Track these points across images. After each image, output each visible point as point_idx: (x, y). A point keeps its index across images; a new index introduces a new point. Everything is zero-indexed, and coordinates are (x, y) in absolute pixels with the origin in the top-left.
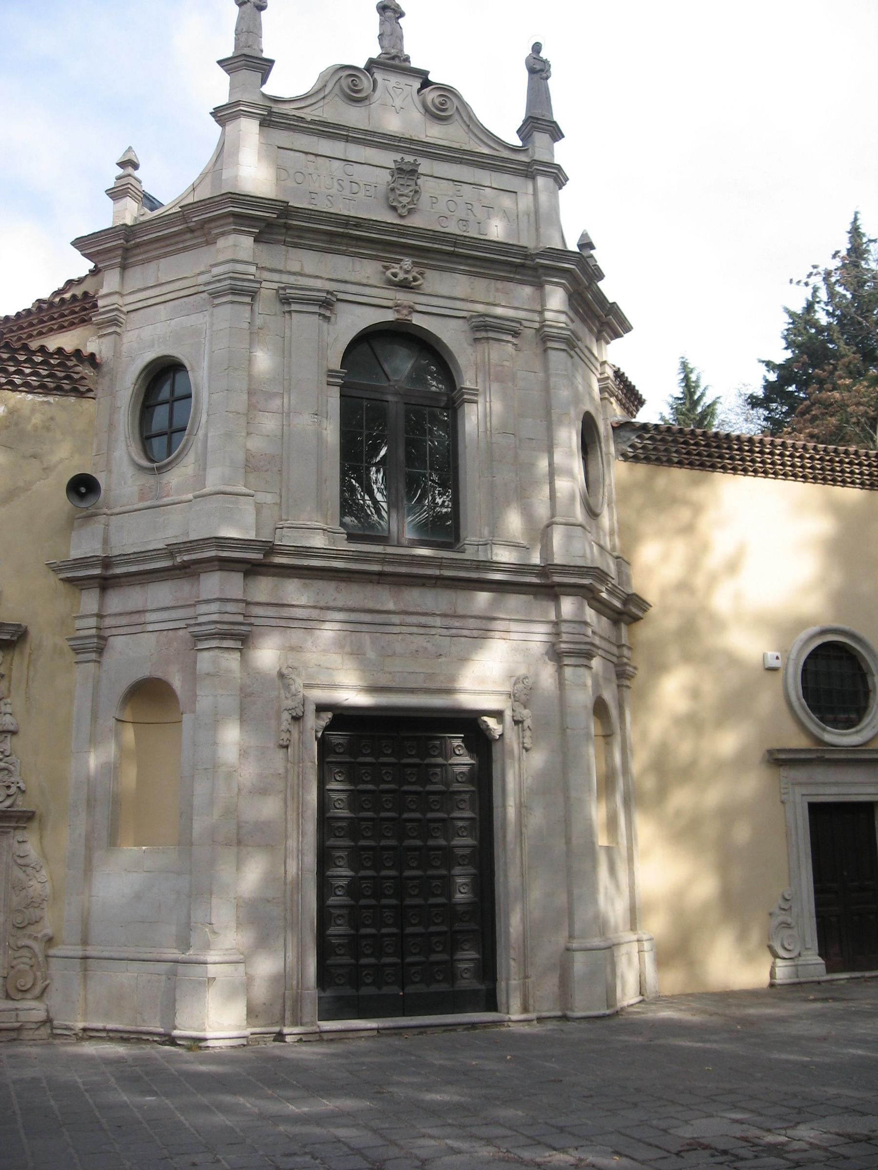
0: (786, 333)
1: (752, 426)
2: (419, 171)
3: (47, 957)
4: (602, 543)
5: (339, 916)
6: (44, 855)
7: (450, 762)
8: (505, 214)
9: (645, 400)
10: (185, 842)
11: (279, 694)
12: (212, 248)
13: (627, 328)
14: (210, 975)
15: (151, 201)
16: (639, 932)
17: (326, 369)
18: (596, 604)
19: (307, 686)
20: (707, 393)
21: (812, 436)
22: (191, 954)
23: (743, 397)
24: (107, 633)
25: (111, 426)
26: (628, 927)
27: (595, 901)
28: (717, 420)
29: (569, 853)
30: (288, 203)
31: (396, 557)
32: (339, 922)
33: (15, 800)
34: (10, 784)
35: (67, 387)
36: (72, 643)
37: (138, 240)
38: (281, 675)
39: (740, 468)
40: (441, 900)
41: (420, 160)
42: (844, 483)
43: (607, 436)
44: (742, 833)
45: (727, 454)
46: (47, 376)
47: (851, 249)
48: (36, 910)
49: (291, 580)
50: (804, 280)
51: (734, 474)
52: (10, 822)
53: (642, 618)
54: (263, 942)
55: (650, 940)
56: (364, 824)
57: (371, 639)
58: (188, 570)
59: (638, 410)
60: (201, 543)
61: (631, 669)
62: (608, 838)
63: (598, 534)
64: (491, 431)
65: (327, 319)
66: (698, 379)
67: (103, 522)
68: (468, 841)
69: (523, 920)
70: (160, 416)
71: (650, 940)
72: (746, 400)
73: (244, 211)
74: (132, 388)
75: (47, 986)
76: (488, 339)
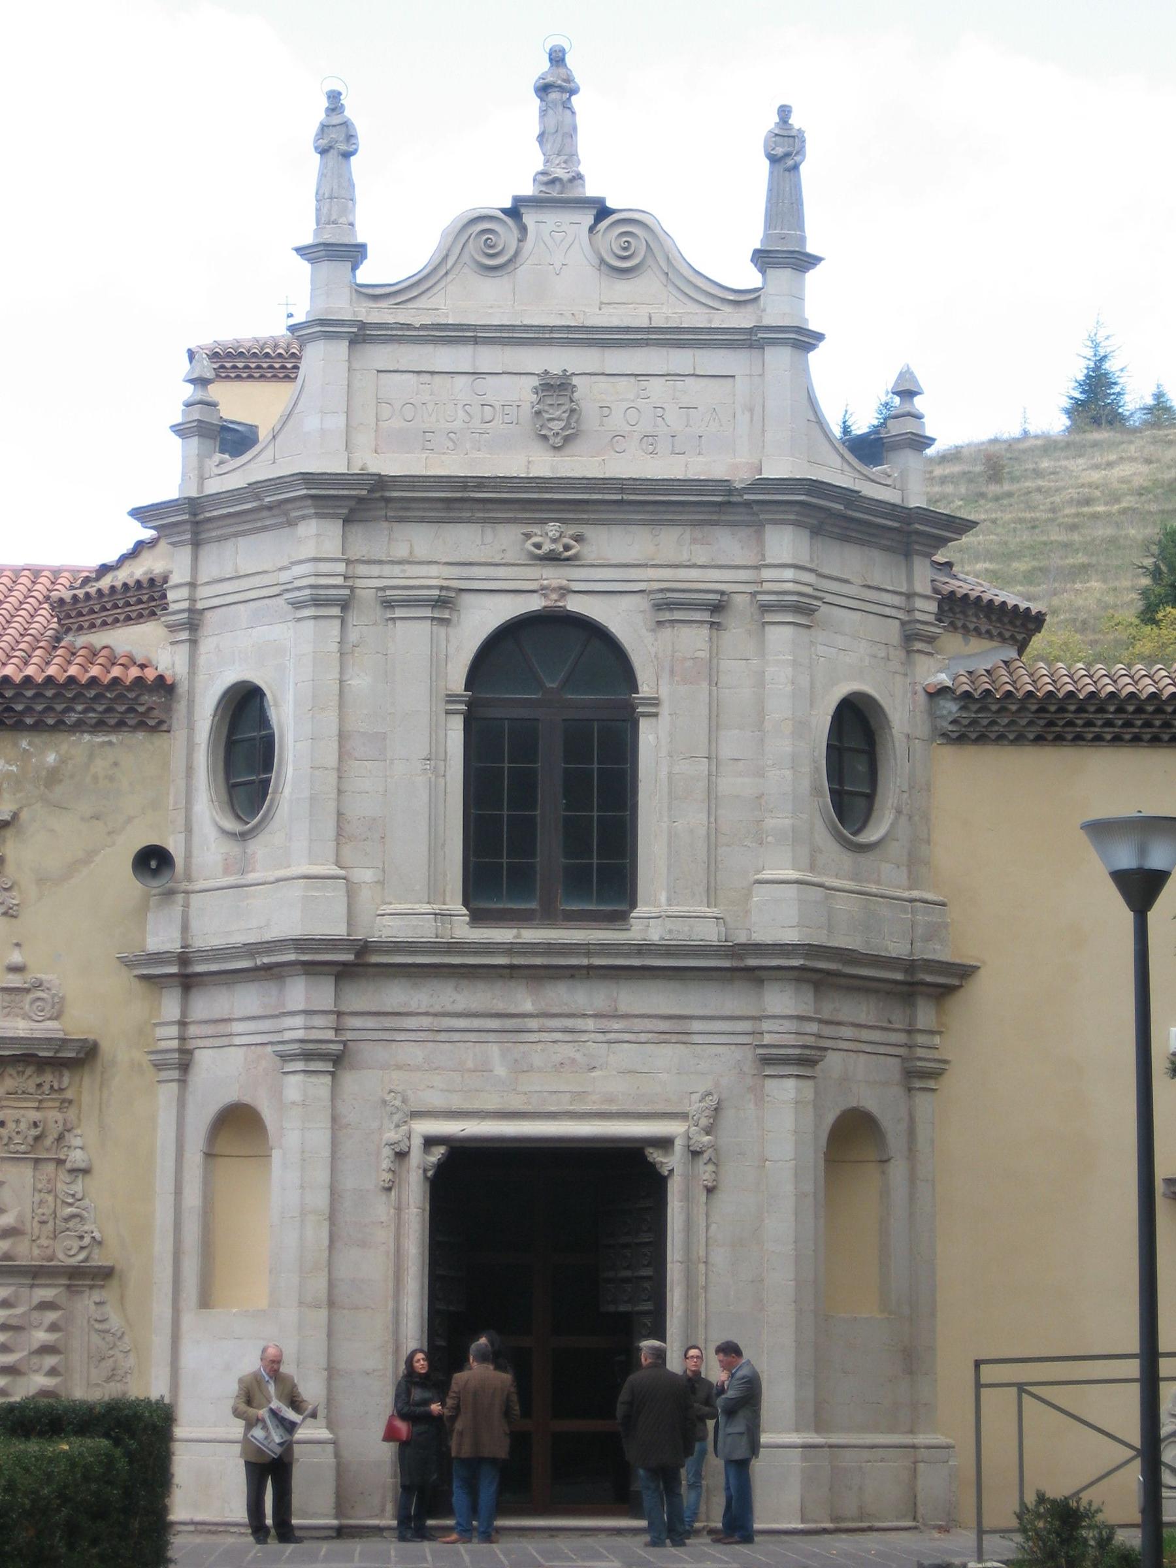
24: (191, 1044)
34: (83, 1234)
36: (153, 1057)
60: (279, 944)
76: (673, 622)
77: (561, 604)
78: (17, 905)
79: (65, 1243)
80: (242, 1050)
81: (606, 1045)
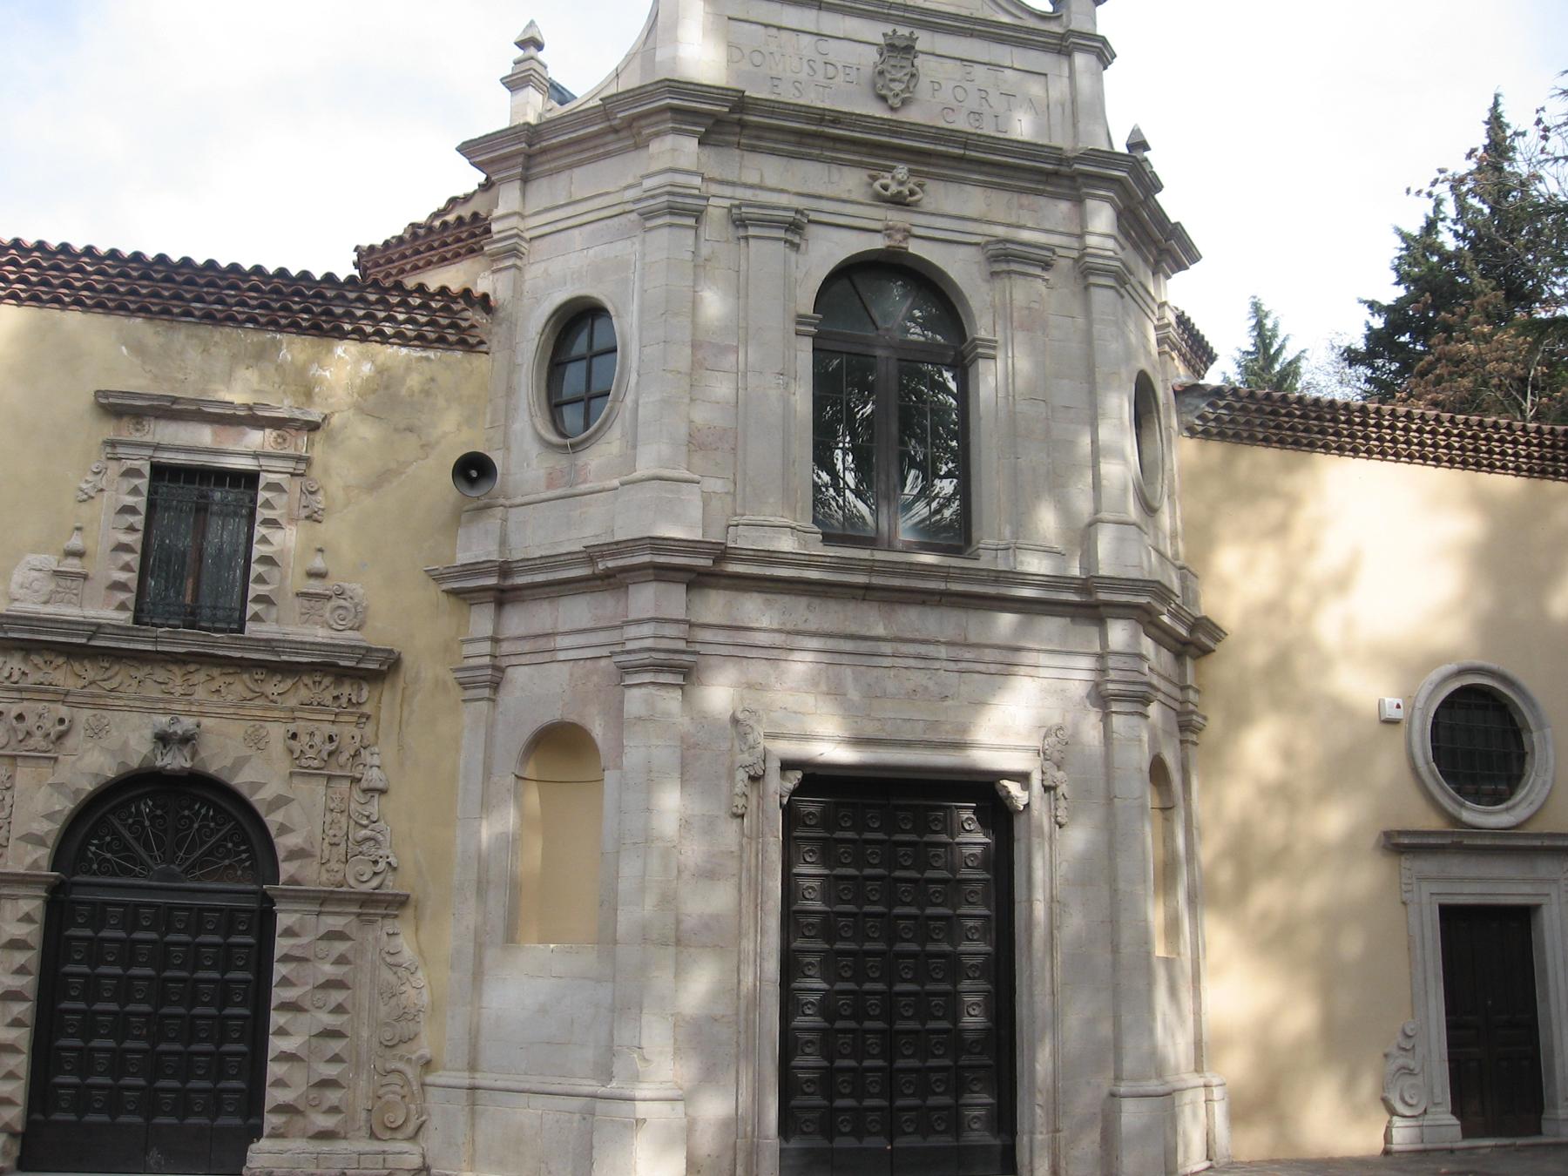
0: (1396, 262)
1: (1348, 390)
2: (917, 48)
3: (423, 1085)
4: (1161, 548)
5: (808, 1042)
6: (421, 953)
7: (957, 840)
8: (1031, 103)
9: (1216, 355)
10: (607, 940)
11: (732, 745)
12: (643, 154)
13: (1194, 256)
14: (640, 1115)
15: (559, 91)
16: (1207, 1074)
17: (793, 315)
18: (1153, 630)
19: (768, 736)
20: (1288, 344)
21: (1435, 404)
22: (613, 1087)
23: (1336, 351)
24: (504, 662)
25: (510, 391)
26: (1192, 1067)
27: (1151, 1031)
28: (1300, 382)
29: (1115, 966)
30: (744, 92)
31: (888, 565)
32: (807, 1050)
33: (384, 880)
34: (377, 858)
35: (432, 336)
37: (544, 144)
38: (735, 721)
39: (1348, 447)
40: (944, 1025)
41: (918, 33)
42: (1492, 468)
43: (1167, 404)
44: (1352, 945)
45: (1330, 427)
46: (427, 324)
47: (1489, 144)
48: (410, 1024)
49: (747, 595)
50: (1427, 189)
51: (1340, 455)
52: (377, 907)
53: (1214, 651)
54: (709, 1075)
55: (1221, 1085)
56: (842, 922)
57: (853, 673)
58: (612, 580)
59: (1207, 368)
60: (631, 544)
61: (1200, 720)
62: (1166, 946)
63: (1156, 536)
64: (1014, 396)
65: (795, 247)
66: (1276, 326)
67: (500, 515)
68: (982, 947)
69: (1054, 1054)
70: (574, 378)
71: (1221, 1085)
72: (1342, 355)
73: (686, 104)
74: (537, 340)
75: (424, 1122)
76: (1009, 272)
77: (904, 245)
78: (323, 510)
79: (357, 868)
80: (566, 667)
81: (957, 674)
